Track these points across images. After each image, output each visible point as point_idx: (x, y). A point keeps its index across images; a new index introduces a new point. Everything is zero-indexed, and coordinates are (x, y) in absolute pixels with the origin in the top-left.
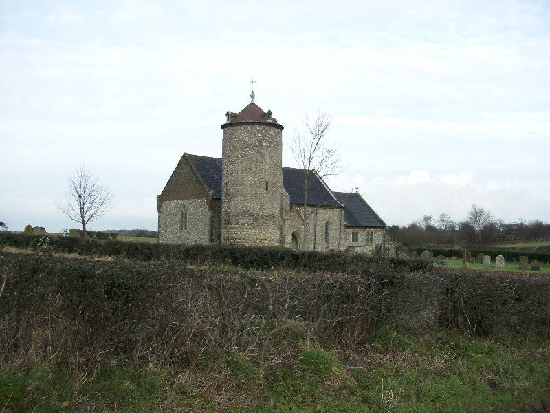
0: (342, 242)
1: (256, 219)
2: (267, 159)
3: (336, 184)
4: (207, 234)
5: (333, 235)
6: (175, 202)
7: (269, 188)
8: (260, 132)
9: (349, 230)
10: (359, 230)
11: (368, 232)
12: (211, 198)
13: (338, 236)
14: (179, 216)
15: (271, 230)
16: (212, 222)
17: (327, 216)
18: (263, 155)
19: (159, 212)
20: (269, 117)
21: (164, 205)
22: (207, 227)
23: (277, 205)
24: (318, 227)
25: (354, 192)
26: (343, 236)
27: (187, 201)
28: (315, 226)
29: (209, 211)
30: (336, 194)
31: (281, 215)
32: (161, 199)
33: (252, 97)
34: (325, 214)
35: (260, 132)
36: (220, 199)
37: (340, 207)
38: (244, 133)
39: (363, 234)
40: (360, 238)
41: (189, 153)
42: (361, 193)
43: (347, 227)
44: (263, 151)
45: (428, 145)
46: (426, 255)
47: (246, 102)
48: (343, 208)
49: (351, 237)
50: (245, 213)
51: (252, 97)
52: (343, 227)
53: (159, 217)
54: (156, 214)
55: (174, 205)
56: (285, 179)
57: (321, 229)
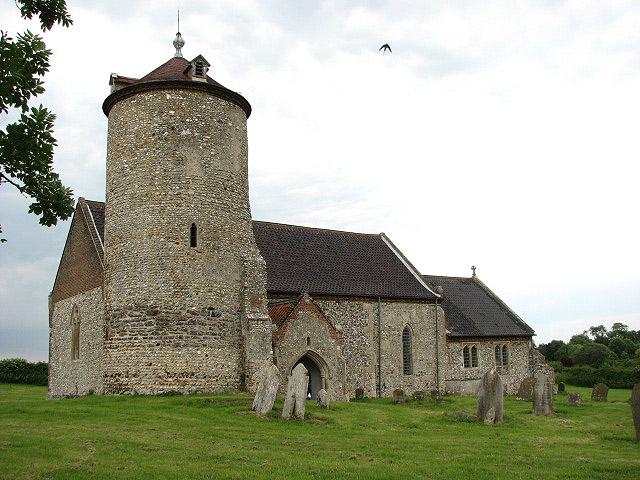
0: (442, 371)
1: (164, 323)
2: (193, 168)
3: (430, 255)
5: (421, 356)
8: (174, 105)
9: (458, 346)
10: (478, 344)
11: (498, 347)
13: (432, 358)
15: (206, 350)
17: (406, 318)
19: (51, 326)
20: (199, 73)
23: (227, 282)
24: (386, 344)
25: (469, 275)
26: (444, 359)
27: (80, 297)
28: (378, 339)
30: (425, 278)
31: (241, 311)
33: (179, 44)
34: (397, 315)
35: (174, 105)
37: (432, 300)
38: (123, 108)
39: (485, 353)
40: (480, 361)
41: (256, 127)
42: (482, 277)
43: (451, 339)
44: (181, 151)
45: (633, 326)
48: (440, 300)
49: (462, 359)
50: (138, 307)
51: (179, 44)
52: (442, 341)
56: (254, 228)
57: (392, 347)
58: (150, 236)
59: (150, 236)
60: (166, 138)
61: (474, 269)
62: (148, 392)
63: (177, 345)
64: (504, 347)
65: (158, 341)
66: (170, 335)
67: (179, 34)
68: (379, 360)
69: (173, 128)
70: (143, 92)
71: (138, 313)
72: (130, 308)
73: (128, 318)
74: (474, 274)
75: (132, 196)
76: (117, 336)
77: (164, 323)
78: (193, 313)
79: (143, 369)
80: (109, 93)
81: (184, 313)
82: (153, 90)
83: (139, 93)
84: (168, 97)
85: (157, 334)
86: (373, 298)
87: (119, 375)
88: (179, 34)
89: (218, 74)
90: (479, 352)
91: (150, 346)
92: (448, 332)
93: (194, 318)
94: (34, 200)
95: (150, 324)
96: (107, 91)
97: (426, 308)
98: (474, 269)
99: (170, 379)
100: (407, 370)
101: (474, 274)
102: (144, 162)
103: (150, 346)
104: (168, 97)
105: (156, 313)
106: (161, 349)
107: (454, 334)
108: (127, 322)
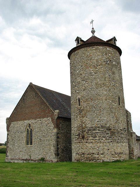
1: (113, 133)
4: (52, 148)
6: (19, 122)
7: (120, 103)
12: (56, 117)
14: (25, 134)
16: (58, 137)
18: (113, 73)
19: (8, 130)
21: (12, 125)
22: (53, 142)
27: (33, 121)
29: (55, 127)
32: (9, 121)
33: (93, 32)
36: (70, 119)
41: (126, 61)
46: (92, 154)
47: (91, 35)
50: (102, 127)
51: (93, 32)
53: (8, 135)
54: (6, 133)
55: (21, 125)
58: (106, 100)
59: (106, 100)
60: (108, 64)
62: (108, 160)
63: (118, 142)
65: (111, 140)
66: (115, 138)
67: (93, 28)
69: (111, 61)
70: (98, 45)
71: (103, 129)
72: (99, 127)
73: (97, 131)
75: (96, 84)
77: (113, 133)
78: (121, 130)
79: (106, 152)
80: (75, 46)
81: (119, 130)
82: (102, 45)
83: (96, 45)
84: (108, 49)
85: (111, 138)
87: (93, 154)
88: (93, 28)
89: (118, 44)
91: (108, 142)
93: (122, 132)
95: (108, 134)
96: (74, 45)
99: (116, 155)
100: (29, 141)
102: (101, 71)
103: (108, 142)
104: (108, 49)
105: (110, 129)
106: (112, 144)
108: (97, 132)
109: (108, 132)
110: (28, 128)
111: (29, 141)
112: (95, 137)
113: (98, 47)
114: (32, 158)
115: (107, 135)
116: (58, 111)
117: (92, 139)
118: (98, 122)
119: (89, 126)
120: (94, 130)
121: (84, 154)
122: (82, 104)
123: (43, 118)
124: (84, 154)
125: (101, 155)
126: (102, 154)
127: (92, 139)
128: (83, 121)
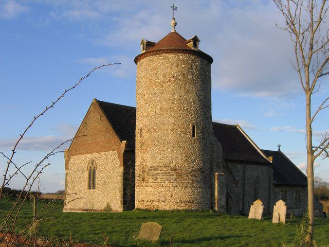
14: (86, 174)
20: (195, 45)
21: (72, 160)
25: (277, 150)
41: (213, 66)
42: (283, 151)
43: (276, 185)
50: (165, 166)
61: (279, 146)
64: (285, 191)
68: (244, 196)
71: (166, 170)
72: (161, 167)
74: (279, 149)
76: (151, 180)
84: (181, 57)
85: (176, 180)
86: (242, 162)
90: (288, 193)
92: (274, 182)
94: (68, 208)
97: (265, 168)
98: (279, 146)
100: (92, 185)
101: (279, 149)
105: (175, 170)
107: (278, 183)
109: (173, 173)
110: (90, 165)
111: (92, 185)
112: (156, 179)
113: (167, 55)
114: (94, 208)
115: (172, 177)
116: (125, 141)
117: (153, 182)
118: (160, 159)
119: (149, 164)
120: (156, 170)
121: (143, 201)
122: (143, 135)
123: (109, 151)
124: (143, 201)
125: (163, 203)
126: (163, 202)
127: (153, 182)
128: (145, 158)
